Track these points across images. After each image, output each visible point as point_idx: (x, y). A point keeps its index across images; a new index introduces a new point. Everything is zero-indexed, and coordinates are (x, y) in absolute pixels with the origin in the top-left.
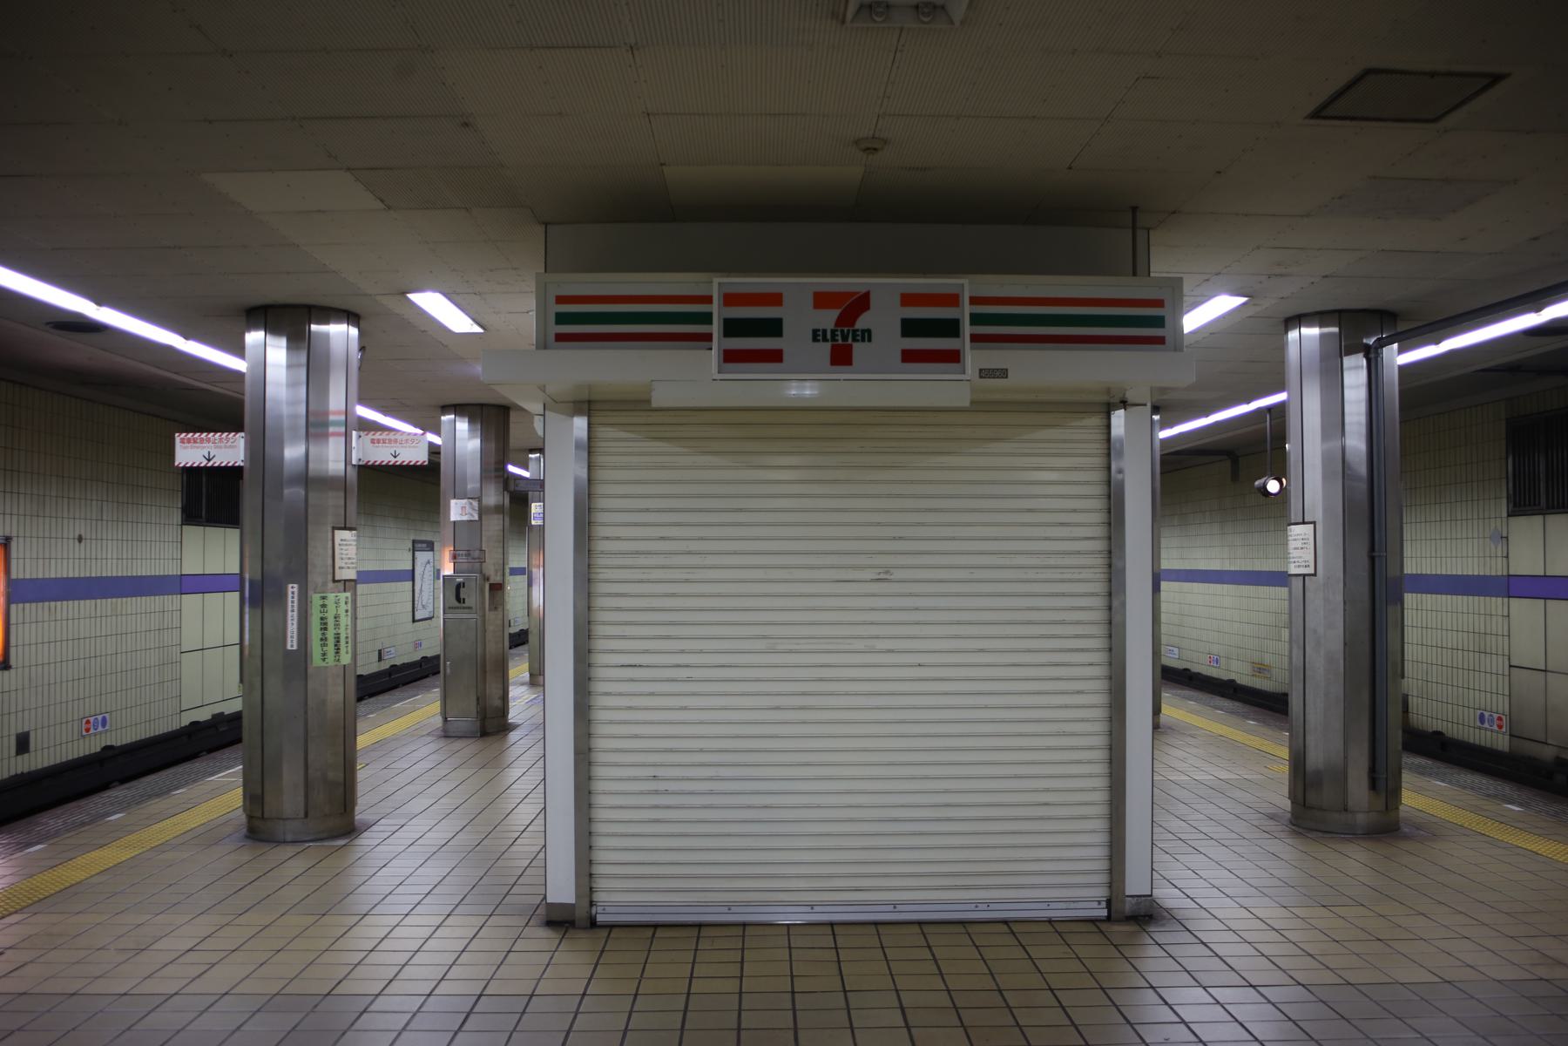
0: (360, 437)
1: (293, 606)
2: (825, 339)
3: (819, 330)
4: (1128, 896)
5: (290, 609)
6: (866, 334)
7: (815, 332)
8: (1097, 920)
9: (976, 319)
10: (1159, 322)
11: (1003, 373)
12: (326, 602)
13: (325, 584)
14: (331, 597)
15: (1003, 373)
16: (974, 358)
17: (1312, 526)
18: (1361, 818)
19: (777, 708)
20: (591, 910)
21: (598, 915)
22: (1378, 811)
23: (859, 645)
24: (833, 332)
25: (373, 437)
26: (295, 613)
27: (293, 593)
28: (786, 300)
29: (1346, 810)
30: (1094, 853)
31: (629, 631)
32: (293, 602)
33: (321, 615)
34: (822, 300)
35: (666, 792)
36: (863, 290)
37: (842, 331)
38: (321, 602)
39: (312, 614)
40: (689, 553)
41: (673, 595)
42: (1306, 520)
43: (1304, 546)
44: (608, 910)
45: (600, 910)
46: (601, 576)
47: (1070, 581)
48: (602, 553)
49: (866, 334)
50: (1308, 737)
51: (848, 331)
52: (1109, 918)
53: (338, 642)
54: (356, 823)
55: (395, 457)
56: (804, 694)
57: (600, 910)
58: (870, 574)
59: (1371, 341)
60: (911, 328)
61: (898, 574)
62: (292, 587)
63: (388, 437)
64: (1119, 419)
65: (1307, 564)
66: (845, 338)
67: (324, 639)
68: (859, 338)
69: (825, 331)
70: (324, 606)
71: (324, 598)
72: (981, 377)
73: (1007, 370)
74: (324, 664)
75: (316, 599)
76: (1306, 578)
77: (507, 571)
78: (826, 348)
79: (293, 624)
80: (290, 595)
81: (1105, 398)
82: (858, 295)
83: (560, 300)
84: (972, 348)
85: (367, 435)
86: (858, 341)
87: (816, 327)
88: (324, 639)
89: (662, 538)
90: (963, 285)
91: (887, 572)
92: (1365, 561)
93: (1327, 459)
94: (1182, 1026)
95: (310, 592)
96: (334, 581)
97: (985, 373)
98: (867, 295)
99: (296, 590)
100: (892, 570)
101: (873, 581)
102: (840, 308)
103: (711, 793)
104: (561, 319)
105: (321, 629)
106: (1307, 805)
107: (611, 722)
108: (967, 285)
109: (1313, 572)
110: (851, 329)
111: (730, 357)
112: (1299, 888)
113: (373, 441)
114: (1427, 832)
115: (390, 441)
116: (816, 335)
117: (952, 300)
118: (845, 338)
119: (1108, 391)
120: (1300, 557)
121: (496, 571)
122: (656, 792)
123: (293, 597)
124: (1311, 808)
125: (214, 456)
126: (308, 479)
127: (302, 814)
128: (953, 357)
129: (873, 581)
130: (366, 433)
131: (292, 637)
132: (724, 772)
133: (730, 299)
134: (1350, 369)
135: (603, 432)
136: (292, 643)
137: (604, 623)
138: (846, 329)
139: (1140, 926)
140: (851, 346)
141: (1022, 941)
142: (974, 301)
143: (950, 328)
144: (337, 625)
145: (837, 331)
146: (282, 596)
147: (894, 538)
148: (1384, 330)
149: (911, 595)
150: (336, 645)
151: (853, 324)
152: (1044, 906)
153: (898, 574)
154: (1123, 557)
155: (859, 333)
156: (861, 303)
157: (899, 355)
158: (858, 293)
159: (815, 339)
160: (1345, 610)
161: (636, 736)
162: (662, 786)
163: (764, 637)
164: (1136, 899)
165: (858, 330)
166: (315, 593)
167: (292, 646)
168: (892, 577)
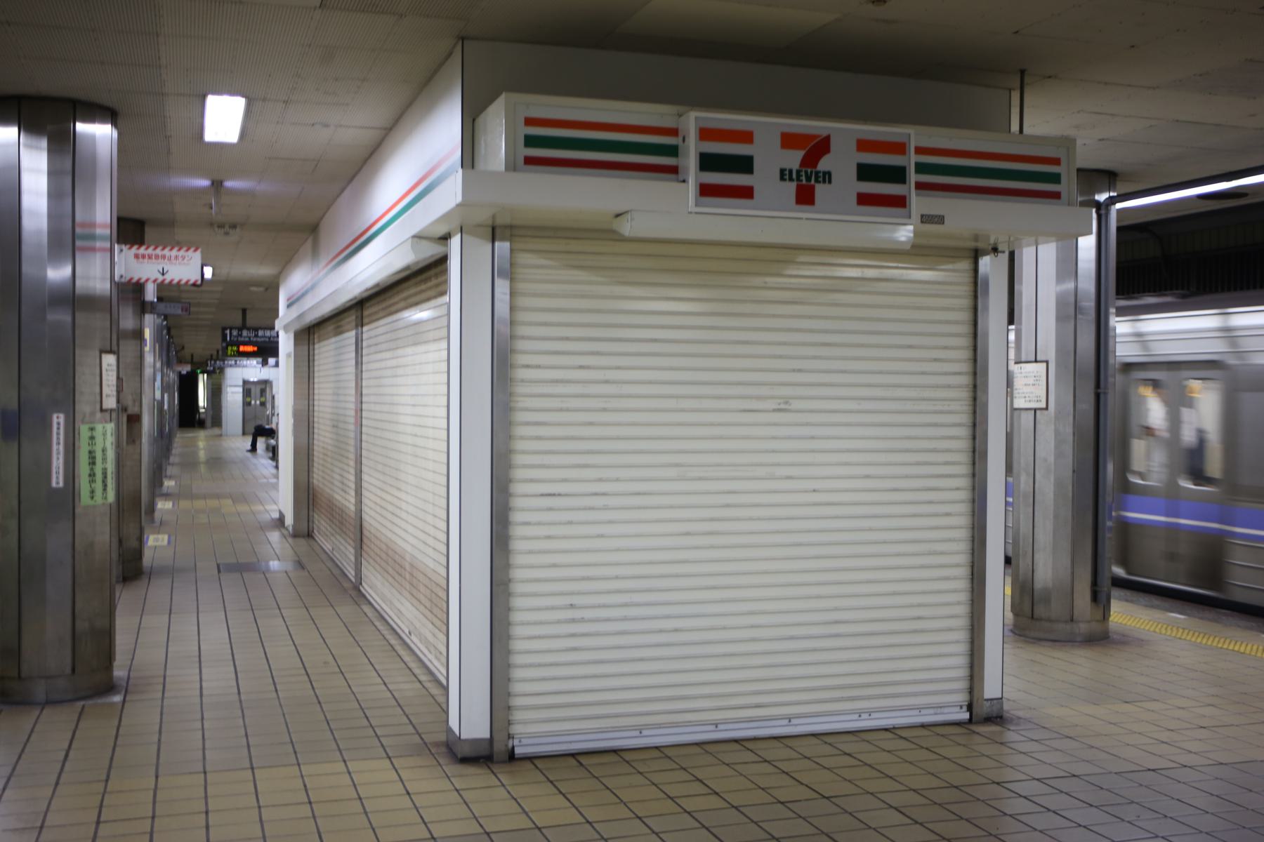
1: (58, 439)
2: (791, 179)
3: (785, 170)
4: (987, 700)
7: (782, 171)
8: (894, 728)
9: (921, 168)
10: (530, 141)
11: (940, 220)
12: (94, 434)
13: (93, 414)
14: (99, 427)
15: (940, 220)
16: (919, 203)
17: (1045, 364)
18: (1083, 628)
19: (688, 534)
20: (508, 742)
21: (516, 748)
23: (761, 472)
24: (798, 172)
26: (61, 448)
27: (59, 424)
28: (756, 138)
29: (1072, 620)
30: (957, 663)
31: (548, 460)
33: (90, 448)
34: (789, 141)
35: (582, 620)
36: (825, 134)
39: (79, 447)
40: (607, 382)
41: (591, 424)
42: (1038, 359)
43: (1036, 382)
44: (525, 741)
45: (516, 742)
46: (520, 405)
47: (941, 412)
48: (523, 381)
50: (1036, 556)
51: (811, 172)
52: (970, 721)
54: (115, 680)
56: (712, 520)
57: (516, 742)
58: (771, 405)
59: (1102, 197)
60: (865, 173)
61: (796, 405)
63: (154, 253)
64: (985, 263)
67: (92, 475)
68: (821, 179)
70: (92, 438)
72: (922, 222)
74: (91, 503)
75: (84, 430)
76: (1038, 412)
78: (791, 187)
81: (972, 244)
82: (818, 139)
83: (529, 122)
84: (917, 195)
85: (130, 248)
86: (820, 182)
88: (92, 475)
89: (581, 367)
90: (909, 135)
91: (786, 403)
92: (1092, 398)
93: (1061, 302)
96: (102, 410)
97: (926, 219)
100: (791, 401)
101: (774, 410)
102: (805, 149)
103: (625, 619)
104: (530, 141)
106: (1035, 617)
107: (530, 552)
108: (915, 136)
109: (1044, 406)
110: (814, 170)
111: (706, 191)
113: (136, 256)
114: (1122, 641)
116: (784, 175)
117: (900, 148)
118: (808, 179)
119: (976, 238)
120: (1032, 393)
121: (134, 401)
122: (573, 621)
124: (1040, 619)
125: (167, 271)
126: (70, 299)
127: (68, 670)
128: (899, 202)
129: (774, 410)
130: (128, 246)
131: (58, 473)
132: (637, 598)
133: (706, 134)
135: (524, 258)
136: (57, 480)
137: (524, 452)
138: (809, 170)
140: (813, 188)
141: (561, 790)
142: (919, 150)
143: (898, 175)
144: (104, 460)
146: (47, 426)
147: (794, 371)
148: (1111, 188)
149: (807, 424)
151: (815, 166)
152: (916, 712)
153: (796, 405)
154: (986, 391)
155: (821, 174)
156: (820, 147)
157: (854, 199)
158: (818, 136)
159: (782, 178)
160: (1074, 441)
161: (554, 566)
162: (577, 614)
163: (677, 465)
164: (989, 702)
165: (820, 172)
167: (58, 483)
168: (790, 407)
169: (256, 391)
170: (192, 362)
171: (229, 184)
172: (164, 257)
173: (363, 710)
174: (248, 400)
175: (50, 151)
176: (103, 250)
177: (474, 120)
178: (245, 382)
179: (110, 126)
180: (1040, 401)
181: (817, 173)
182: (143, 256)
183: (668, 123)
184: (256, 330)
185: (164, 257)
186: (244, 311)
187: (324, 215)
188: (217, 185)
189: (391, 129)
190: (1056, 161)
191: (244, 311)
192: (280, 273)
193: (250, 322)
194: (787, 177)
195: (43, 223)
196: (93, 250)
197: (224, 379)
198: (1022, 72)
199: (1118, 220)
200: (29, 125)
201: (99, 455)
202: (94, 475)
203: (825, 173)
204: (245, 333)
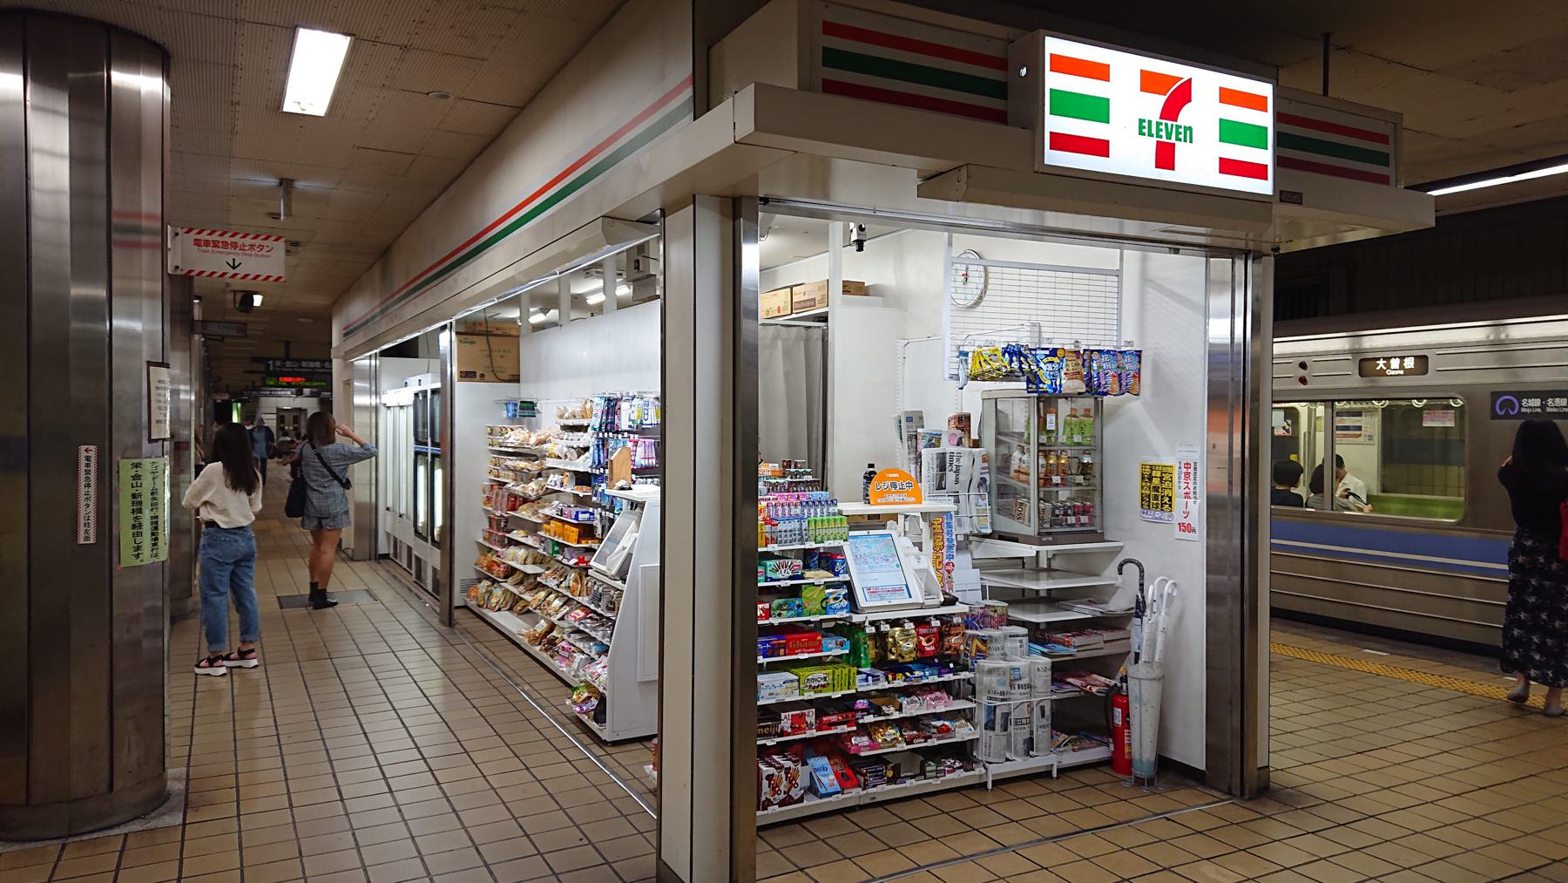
0: (177, 234)
1: (88, 479)
2: (1151, 135)
3: (1144, 121)
5: (82, 482)
6: (1188, 132)
22: (289, 571)
25: (198, 237)
27: (88, 458)
32: (87, 472)
33: (133, 491)
38: (133, 472)
49: (1188, 132)
53: (156, 528)
55: (234, 268)
62: (86, 450)
66: (1169, 137)
68: (1181, 136)
70: (137, 477)
71: (137, 466)
73: (1301, 194)
74: (138, 562)
75: (125, 469)
77: (1335, 429)
79: (88, 506)
80: (83, 462)
83: (830, 28)
88: (137, 526)
94: (539, 779)
95: (116, 457)
99: (93, 454)
105: (133, 511)
110: (1174, 123)
112: (1480, 747)
113: (197, 242)
115: (225, 244)
118: (1169, 137)
123: (88, 465)
136: (87, 533)
140: (1173, 145)
145: (1161, 124)
150: (153, 534)
155: (1182, 130)
156: (1179, 97)
165: (1180, 127)
166: (123, 458)
167: (87, 538)
169: (289, 418)
170: (230, 393)
171: (300, 185)
172: (235, 245)
173: (394, 709)
174: (282, 425)
175: (74, 119)
176: (151, 246)
177: (709, 48)
178: (279, 410)
179: (161, 79)
181: (1179, 127)
182: (207, 243)
183: (993, 50)
184: (300, 361)
185: (235, 245)
186: (287, 343)
187: (397, 238)
188: (286, 184)
189: (522, 109)
190: (1383, 139)
191: (287, 343)
192: (333, 304)
193: (293, 355)
194: (1145, 131)
196: (138, 245)
197: (258, 407)
200: (40, 71)
201: (146, 500)
202: (140, 525)
204: (288, 364)
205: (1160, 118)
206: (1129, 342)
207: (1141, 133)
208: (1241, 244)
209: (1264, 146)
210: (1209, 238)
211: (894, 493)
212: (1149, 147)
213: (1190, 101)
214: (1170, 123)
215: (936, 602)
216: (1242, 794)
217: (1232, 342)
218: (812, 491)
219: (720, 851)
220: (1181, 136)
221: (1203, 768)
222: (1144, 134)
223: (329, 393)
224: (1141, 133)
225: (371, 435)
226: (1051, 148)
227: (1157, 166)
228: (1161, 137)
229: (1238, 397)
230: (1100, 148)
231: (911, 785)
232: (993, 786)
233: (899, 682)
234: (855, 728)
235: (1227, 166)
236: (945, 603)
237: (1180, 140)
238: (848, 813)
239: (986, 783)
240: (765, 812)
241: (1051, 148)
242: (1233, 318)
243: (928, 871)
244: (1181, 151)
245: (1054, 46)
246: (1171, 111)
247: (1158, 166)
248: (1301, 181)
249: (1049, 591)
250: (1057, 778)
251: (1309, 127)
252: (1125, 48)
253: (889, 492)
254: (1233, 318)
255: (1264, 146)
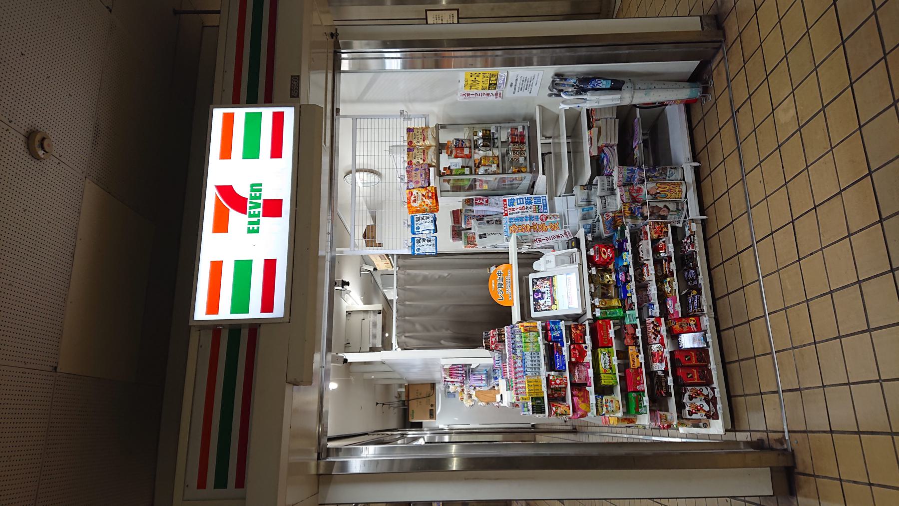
2: (258, 223)
3: (249, 228)
6: (254, 188)
7: (250, 231)
37: (251, 208)
43: (440, 19)
49: (254, 188)
51: (251, 203)
65: (451, 16)
66: (258, 206)
68: (258, 194)
69: (250, 223)
73: (292, 76)
76: (460, 16)
83: (202, 484)
87: (246, 230)
98: (219, 188)
110: (249, 200)
116: (253, 230)
118: (258, 206)
134: (349, 61)
139: (693, 130)
140: (265, 201)
156: (227, 192)
158: (217, 197)
180: (453, 15)
194: (256, 227)
195: (622, 361)
198: (176, 12)
199: (435, 344)
203: (252, 190)
205: (246, 214)
206: (401, 113)
207: (257, 231)
208: (331, 55)
209: (250, 262)
210: (329, 71)
211: (505, 286)
212: (267, 223)
213: (231, 187)
214: (249, 205)
215: (578, 254)
216: (720, 41)
217: (399, 58)
218: (504, 335)
219: (749, 475)
220: (258, 194)
221: (699, 62)
222: (258, 228)
223: (445, 41)
224: (257, 231)
225: (462, 57)
226: (272, 311)
227: (280, 216)
228: (259, 212)
229: (436, 54)
230: (270, 266)
231: (703, 280)
232: (705, 216)
233: (628, 246)
234: (663, 319)
235: (276, 152)
236: (578, 246)
237: (260, 195)
238: (695, 153)
239: (702, 220)
240: (702, 284)
241: (272, 311)
242: (386, 58)
243: (731, 82)
244: (269, 194)
245: (200, 313)
246: (240, 204)
247: (280, 215)
248: (282, 84)
249: (568, 137)
250: (699, 162)
251: (215, 381)
252: (202, 204)
253: (505, 289)
254: (386, 58)
255: (250, 262)
